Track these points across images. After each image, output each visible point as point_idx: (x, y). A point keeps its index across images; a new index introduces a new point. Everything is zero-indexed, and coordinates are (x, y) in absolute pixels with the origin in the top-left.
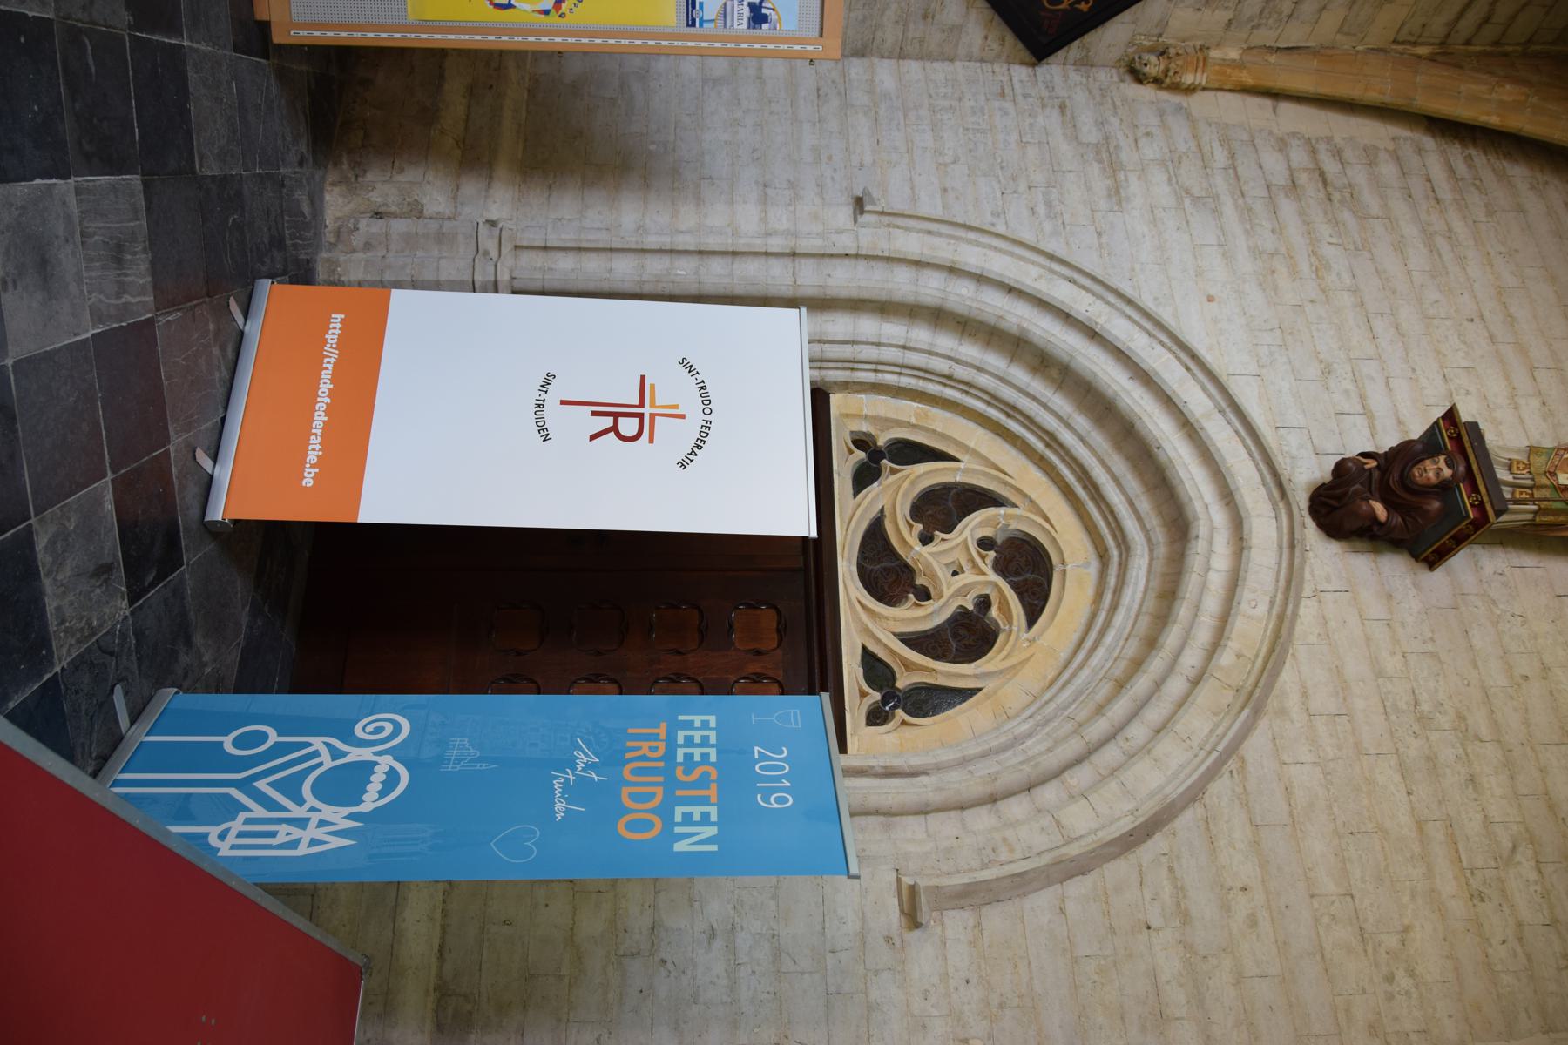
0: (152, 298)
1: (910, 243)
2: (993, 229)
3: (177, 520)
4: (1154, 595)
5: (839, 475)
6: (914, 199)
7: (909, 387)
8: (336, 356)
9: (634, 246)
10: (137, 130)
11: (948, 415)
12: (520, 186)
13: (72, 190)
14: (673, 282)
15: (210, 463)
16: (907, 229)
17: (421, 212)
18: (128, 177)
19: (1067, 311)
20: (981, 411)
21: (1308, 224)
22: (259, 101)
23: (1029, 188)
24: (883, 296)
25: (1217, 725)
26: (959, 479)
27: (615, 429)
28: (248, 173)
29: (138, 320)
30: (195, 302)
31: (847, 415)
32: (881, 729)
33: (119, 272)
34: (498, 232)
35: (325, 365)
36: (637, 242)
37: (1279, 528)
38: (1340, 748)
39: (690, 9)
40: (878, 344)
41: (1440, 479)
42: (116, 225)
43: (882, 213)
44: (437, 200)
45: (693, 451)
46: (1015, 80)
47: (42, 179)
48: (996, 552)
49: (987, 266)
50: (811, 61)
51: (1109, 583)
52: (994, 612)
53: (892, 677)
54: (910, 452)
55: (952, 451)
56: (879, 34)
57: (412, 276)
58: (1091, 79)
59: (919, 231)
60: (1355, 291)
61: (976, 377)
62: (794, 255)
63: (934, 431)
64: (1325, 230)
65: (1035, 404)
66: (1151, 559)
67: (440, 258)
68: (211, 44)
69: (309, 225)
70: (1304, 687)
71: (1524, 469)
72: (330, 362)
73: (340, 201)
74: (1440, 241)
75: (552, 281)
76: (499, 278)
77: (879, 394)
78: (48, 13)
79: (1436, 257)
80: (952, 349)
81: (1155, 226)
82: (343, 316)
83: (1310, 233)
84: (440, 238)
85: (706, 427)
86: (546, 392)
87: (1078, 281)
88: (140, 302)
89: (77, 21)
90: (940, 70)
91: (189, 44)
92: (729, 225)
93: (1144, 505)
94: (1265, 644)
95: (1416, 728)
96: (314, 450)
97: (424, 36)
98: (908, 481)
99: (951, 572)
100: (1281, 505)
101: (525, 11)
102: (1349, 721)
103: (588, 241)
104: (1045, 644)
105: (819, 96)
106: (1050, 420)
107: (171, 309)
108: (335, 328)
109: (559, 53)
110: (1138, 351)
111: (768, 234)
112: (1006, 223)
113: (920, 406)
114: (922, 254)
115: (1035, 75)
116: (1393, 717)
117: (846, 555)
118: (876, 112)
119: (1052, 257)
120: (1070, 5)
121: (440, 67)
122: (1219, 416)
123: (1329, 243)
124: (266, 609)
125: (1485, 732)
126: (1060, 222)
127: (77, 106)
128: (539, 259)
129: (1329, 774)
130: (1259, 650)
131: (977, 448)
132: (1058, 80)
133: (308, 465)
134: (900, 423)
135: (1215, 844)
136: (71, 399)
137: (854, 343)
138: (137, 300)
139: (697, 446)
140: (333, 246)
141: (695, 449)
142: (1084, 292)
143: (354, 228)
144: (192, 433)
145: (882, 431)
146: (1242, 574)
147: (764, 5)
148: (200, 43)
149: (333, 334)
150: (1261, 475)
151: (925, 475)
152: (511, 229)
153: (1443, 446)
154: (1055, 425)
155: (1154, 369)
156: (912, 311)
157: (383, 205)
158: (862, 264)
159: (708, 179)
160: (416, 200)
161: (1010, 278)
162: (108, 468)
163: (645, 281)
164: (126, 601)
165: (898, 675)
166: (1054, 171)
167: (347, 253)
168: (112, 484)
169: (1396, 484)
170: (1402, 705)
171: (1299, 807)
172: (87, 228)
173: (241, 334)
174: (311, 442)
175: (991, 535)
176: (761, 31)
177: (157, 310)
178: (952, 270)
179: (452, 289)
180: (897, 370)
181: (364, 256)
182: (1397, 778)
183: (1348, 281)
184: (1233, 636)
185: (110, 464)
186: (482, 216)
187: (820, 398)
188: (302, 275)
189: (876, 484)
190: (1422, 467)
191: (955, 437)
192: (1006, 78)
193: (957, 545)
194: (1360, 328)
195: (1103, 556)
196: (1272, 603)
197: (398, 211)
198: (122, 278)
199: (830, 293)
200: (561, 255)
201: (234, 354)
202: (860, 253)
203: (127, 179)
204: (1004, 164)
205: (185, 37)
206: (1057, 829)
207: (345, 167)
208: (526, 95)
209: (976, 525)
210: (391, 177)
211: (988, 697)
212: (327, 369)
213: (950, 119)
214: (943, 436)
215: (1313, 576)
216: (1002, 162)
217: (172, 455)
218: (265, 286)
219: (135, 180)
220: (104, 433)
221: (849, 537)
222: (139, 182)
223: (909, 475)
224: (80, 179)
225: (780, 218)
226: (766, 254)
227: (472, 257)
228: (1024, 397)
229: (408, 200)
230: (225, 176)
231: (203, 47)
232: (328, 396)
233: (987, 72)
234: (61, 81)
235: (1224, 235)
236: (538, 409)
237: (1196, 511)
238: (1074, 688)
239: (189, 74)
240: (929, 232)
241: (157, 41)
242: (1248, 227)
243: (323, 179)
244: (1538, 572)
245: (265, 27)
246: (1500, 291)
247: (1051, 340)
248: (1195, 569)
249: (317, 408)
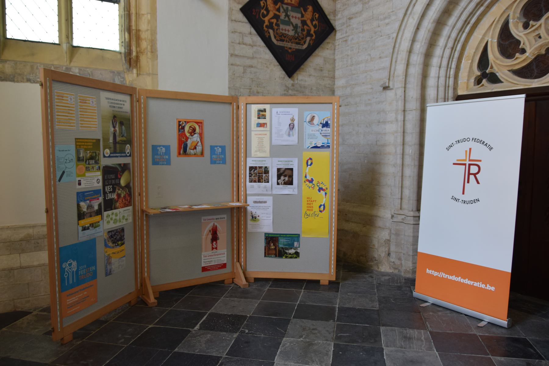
0: (422, 330)
1: (400, 68)
2: (395, 38)
3: (507, 337)
5: (493, 89)
6: (384, 68)
7: (456, 64)
8: (443, 273)
9: (401, 168)
10: (366, 325)
11: (467, 48)
12: (379, 207)
13: (387, 348)
14: (415, 154)
15: (483, 322)
16: (395, 70)
17: (388, 240)
18: (381, 330)
19: (426, 5)
20: (467, 34)
22: (353, 287)
23: (379, 26)
24: (420, 77)
26: (495, 40)
27: (475, 175)
28: (377, 294)
29: (430, 336)
30: (423, 317)
31: (467, 88)
33: (414, 339)
34: (395, 215)
35: (446, 277)
36: (400, 167)
39: (324, 147)
40: (439, 77)
42: (398, 337)
43: (389, 79)
44: (384, 235)
45: (485, 145)
46: (341, 37)
47: (384, 356)
48: (530, 21)
50: (340, 106)
54: (484, 61)
55: (483, 45)
56: (327, 86)
57: (411, 245)
58: (340, 10)
59: (396, 66)
61: (452, 38)
62: (404, 111)
63: (475, 53)
65: (464, 13)
67: (405, 235)
68: (337, 299)
69: (393, 278)
72: (445, 276)
73: (384, 266)
75: (414, 197)
76: (412, 215)
77: (458, 76)
78: (332, 344)
82: (427, 269)
84: (397, 234)
85: (475, 140)
86: (459, 200)
88: (424, 335)
89: (334, 336)
90: (338, 64)
91: (337, 305)
92: (394, 135)
96: (479, 285)
97: (333, 233)
98: (497, 61)
99: (539, 39)
101: (325, 200)
103: (399, 183)
105: (348, 105)
106: (471, 6)
107: (426, 325)
108: (432, 272)
109: (338, 190)
111: (397, 120)
112: (392, 33)
113: (464, 59)
115: (339, 30)
117: (530, 84)
118: (353, 85)
119: (405, 14)
120: (316, 21)
121: (340, 230)
124: (544, 312)
126: (392, 13)
127: (360, 341)
128: (405, 201)
132: (340, 22)
133: (486, 288)
134: (471, 67)
136: (461, 363)
137: (438, 87)
138: (423, 335)
139: (483, 143)
140: (399, 271)
141: (484, 144)
143: (393, 263)
144: (472, 326)
145: (474, 73)
147: (322, 123)
148: (337, 302)
149: (434, 273)
151: (494, 55)
152: (394, 210)
154: (473, 4)
156: (426, 65)
157: (386, 252)
158: (407, 86)
159: (377, 142)
160: (384, 242)
161: (413, 29)
162: (487, 356)
163: (414, 164)
164: (543, 361)
166: (373, 18)
167: (402, 266)
168: (493, 356)
172: (399, 346)
173: (433, 304)
174: (476, 286)
176: (331, 124)
177: (426, 330)
178: (410, 52)
179: (418, 232)
180: (449, 69)
181: (403, 260)
185: (485, 355)
186: (390, 220)
187: (459, 98)
188: (412, 282)
189: (497, 74)
191: (477, 44)
192: (341, 40)
197: (388, 248)
198: (416, 338)
199: (419, 96)
200: (404, 194)
201: (441, 308)
202: (404, 87)
203: (382, 331)
204: (371, 37)
205: (335, 306)
207: (372, 264)
208: (348, 203)
209: (517, 31)
210: (376, 249)
212: (447, 277)
213: (355, 58)
214: (477, 48)
216: (370, 38)
217: (481, 334)
218: (415, 294)
219: (382, 329)
220: (473, 355)
221: (521, 83)
222: (383, 327)
223: (494, 61)
224: (383, 345)
225: (391, 116)
226: (404, 121)
227: (404, 224)
228: (461, 18)
229: (384, 244)
230: (378, 301)
231: (338, 301)
232: (458, 278)
233: (338, 47)
234: (352, 344)
236: (466, 203)
239: (347, 307)
240: (396, 62)
241: (337, 314)
243: (377, 271)
245: (330, 282)
247: (438, 10)
249: (463, 282)
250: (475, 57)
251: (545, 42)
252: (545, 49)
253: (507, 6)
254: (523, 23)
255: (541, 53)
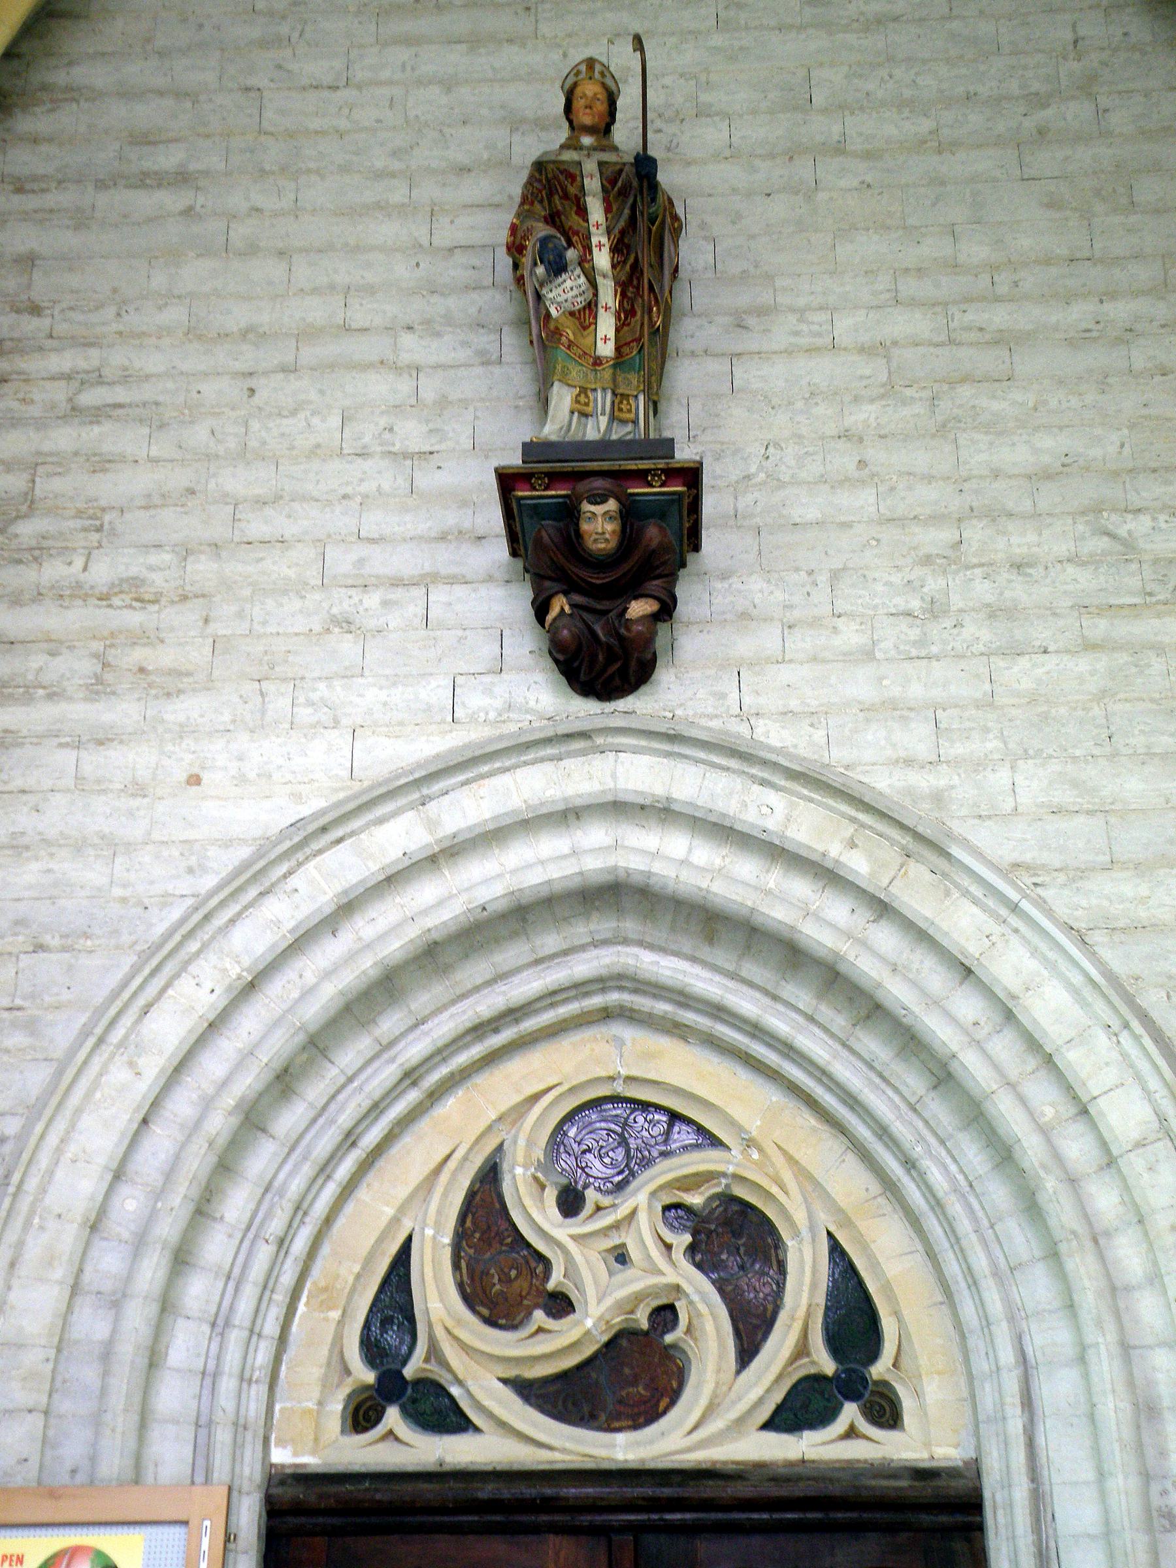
4: (707, 949)
21: (40, 594)
25: (966, 893)
32: (908, 1404)
37: (636, 751)
38: (986, 730)
41: (618, 516)
49: (101, 1160)
51: (666, 1012)
52: (695, 1200)
53: (816, 1380)
55: (393, 1248)
60: (186, 552)
63: (358, 1277)
64: (54, 571)
66: (641, 943)
70: (897, 761)
71: (587, 397)
74: (90, 397)
79: (120, 412)
80: (230, 1236)
81: (27, 848)
83: (61, 596)
87: (150, 999)
93: (550, 942)
94: (835, 804)
95: (948, 623)
98: (457, 1332)
100: (599, 741)
102: (944, 710)
104: (759, 1123)
110: (300, 916)
114: (61, 1283)
116: (934, 649)
122: (432, 806)
123: (85, 569)
125: (946, 535)
129: (1026, 751)
130: (843, 815)
131: (398, 1203)
135: (1145, 924)
142: (170, 992)
146: (712, 818)
150: (542, 760)
153: (561, 500)
155: (337, 896)
161: (130, 1120)
165: (813, 1371)
169: (602, 575)
170: (914, 634)
171: (1079, 800)
175: (556, 1193)
182: (1024, 662)
183: (167, 557)
184: (820, 848)
190: (595, 536)
193: (583, 1255)
194: (262, 559)
195: (606, 1015)
196: (763, 783)
206: (1149, 1148)
211: (847, 1222)
215: (716, 716)
235: (57, 736)
237: (601, 869)
238: (866, 1090)
242: (41, 692)
244: (696, 407)
246: (193, 333)
248: (704, 885)
250: (356, 1297)
251: (655, 1286)
252: (648, 1310)
253: (503, 1107)
254: (559, 1188)
255: (634, 1325)
